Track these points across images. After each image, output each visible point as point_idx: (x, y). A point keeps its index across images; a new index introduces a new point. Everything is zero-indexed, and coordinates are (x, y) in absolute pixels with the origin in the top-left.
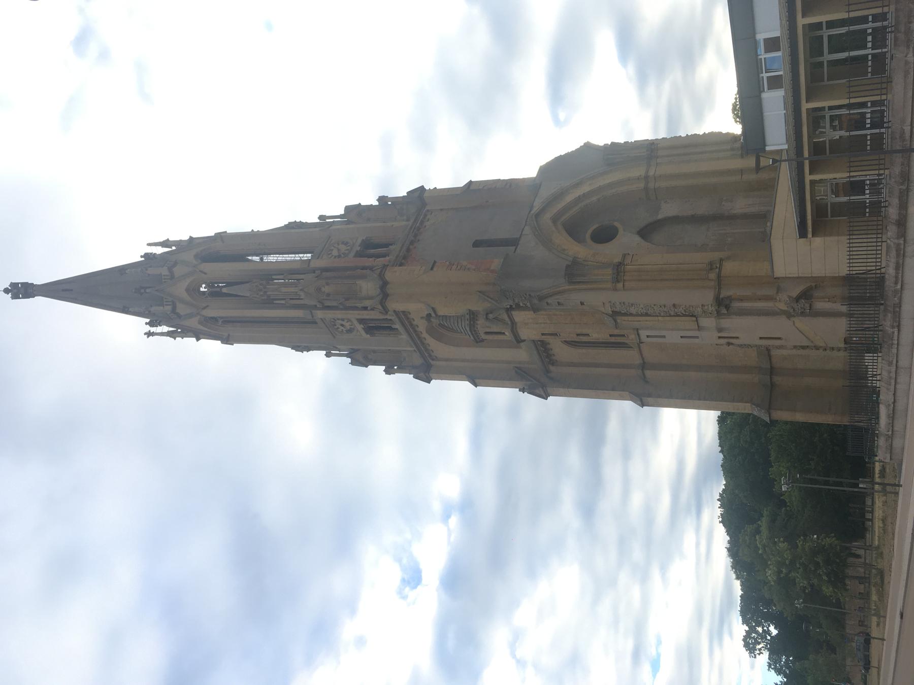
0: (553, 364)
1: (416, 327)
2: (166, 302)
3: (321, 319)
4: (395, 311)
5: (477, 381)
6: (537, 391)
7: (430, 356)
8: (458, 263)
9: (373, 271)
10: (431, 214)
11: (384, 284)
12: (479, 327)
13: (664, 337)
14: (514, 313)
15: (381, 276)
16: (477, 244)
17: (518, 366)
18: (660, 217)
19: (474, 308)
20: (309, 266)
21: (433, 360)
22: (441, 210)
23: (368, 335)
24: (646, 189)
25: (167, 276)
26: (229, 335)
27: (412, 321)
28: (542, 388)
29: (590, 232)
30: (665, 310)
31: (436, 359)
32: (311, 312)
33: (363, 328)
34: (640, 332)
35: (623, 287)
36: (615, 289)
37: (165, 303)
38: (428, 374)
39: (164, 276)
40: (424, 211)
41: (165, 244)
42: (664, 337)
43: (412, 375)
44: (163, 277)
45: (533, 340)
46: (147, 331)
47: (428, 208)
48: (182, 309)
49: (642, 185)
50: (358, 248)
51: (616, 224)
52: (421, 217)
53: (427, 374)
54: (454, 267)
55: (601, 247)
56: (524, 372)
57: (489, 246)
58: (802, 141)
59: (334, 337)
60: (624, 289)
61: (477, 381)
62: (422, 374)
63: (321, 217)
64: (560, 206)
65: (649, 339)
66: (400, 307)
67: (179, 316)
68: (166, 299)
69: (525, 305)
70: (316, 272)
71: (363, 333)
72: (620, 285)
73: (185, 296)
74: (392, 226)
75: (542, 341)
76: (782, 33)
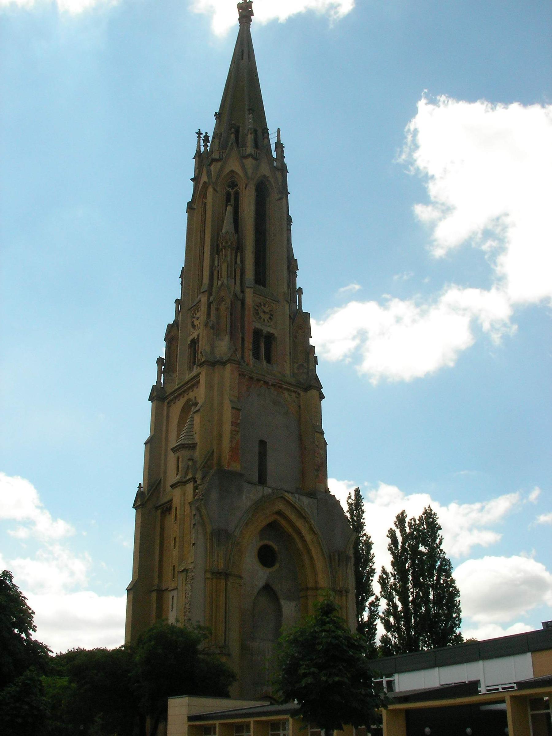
0: (162, 513)
1: (196, 387)
2: (223, 152)
3: (200, 301)
4: (200, 373)
5: (149, 445)
6: (139, 500)
7: (171, 401)
8: (237, 431)
9: (235, 352)
10: (296, 397)
11: (223, 363)
12: (183, 452)
13: (172, 610)
14: (192, 483)
15: (229, 361)
16: (263, 443)
17: (162, 482)
18: (282, 602)
19: (198, 448)
20: (247, 287)
21: (168, 403)
22: (300, 406)
23: (189, 342)
24: (307, 589)
25: (246, 153)
26: (194, 209)
27: (183, 396)
28: (141, 505)
29: (271, 543)
30: (187, 612)
31: (169, 407)
32: (206, 291)
33: (194, 338)
34: (176, 591)
35: (208, 578)
36: (206, 572)
37: (221, 151)
38: (156, 399)
39: (246, 149)
40: (299, 391)
41: (280, 146)
42: (172, 610)
43: (155, 384)
44: (244, 149)
45: (172, 500)
46: (202, 131)
47: (302, 393)
48: (214, 168)
49: (311, 584)
50: (264, 331)
51: (277, 565)
52: (292, 389)
53: (155, 398)
54: (234, 428)
55: (255, 552)
56: (156, 487)
57: (260, 453)
58: (229, 718)
59: (189, 310)
60: (206, 579)
61: (149, 445)
62: (155, 394)
63: (300, 290)
64: (293, 517)
65: (171, 597)
66: (203, 379)
67: (210, 165)
68: (225, 152)
69: (197, 494)
70: (242, 294)
71: (191, 338)
72: (209, 575)
73: (227, 170)
74: (286, 362)
75: (171, 508)
76: (269, 701)
